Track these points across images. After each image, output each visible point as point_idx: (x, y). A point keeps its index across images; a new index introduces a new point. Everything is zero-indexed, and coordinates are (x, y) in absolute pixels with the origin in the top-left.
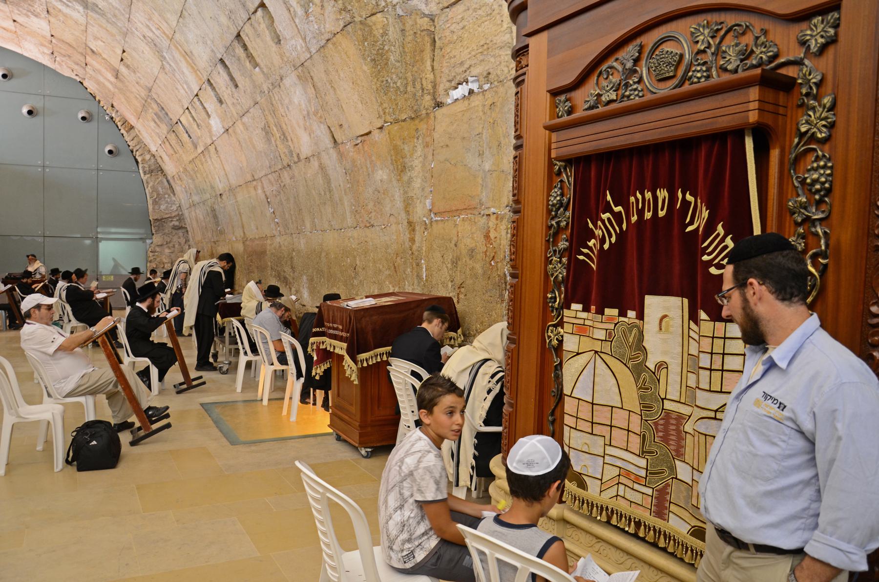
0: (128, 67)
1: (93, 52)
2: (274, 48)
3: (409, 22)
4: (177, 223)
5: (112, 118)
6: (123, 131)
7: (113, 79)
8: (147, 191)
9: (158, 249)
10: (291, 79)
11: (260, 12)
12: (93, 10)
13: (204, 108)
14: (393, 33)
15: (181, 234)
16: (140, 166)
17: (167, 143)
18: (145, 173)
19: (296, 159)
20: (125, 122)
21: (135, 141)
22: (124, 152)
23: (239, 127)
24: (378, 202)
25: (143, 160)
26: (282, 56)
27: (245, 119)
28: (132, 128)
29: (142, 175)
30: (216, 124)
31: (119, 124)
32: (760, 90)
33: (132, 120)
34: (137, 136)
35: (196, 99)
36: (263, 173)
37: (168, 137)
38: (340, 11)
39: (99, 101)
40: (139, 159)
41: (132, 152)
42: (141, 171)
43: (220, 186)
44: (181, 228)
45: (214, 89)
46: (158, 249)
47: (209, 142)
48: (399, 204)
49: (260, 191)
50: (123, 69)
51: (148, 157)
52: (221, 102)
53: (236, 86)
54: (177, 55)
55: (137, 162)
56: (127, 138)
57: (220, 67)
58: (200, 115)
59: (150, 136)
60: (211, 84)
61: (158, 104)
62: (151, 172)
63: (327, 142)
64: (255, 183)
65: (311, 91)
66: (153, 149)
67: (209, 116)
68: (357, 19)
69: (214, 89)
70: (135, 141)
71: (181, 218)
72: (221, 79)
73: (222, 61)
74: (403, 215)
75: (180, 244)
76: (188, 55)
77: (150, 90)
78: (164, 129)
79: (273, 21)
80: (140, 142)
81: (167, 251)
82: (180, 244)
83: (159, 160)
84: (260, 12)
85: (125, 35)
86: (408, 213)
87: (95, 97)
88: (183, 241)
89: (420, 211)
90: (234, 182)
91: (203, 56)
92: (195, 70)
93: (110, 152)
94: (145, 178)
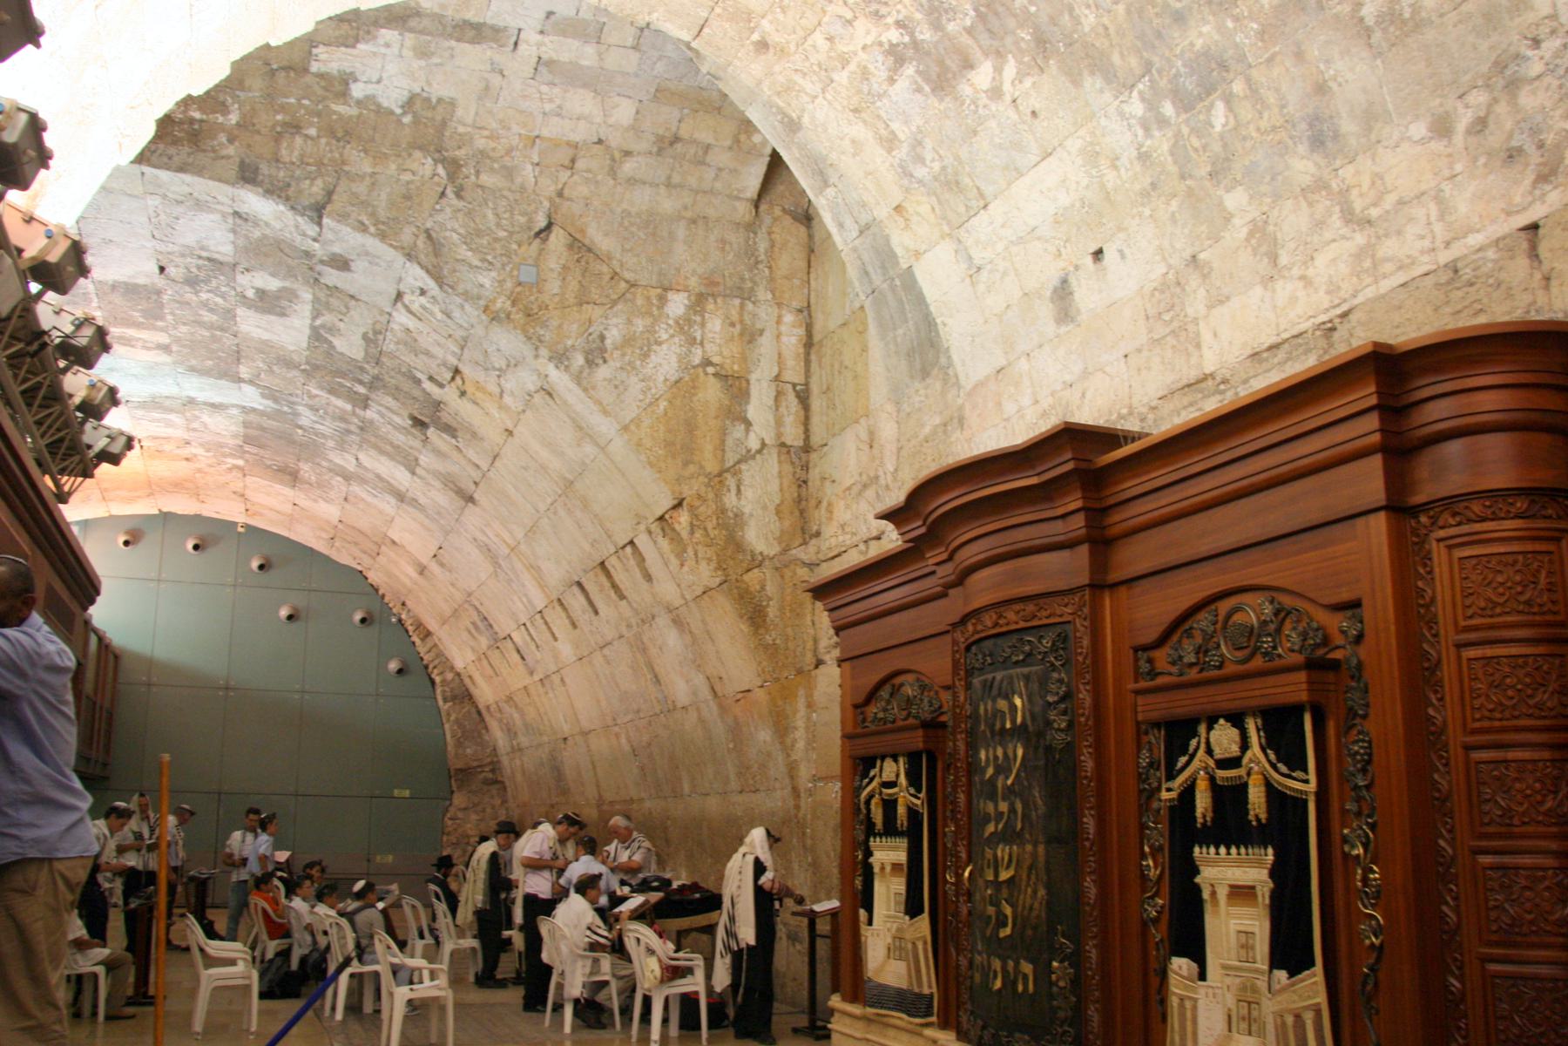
0: (442, 565)
1: (394, 542)
2: (645, 585)
3: (788, 573)
4: (490, 776)
5: (400, 620)
6: (415, 638)
7: (414, 575)
8: (447, 726)
9: (460, 815)
10: (663, 621)
11: (629, 549)
12: (409, 504)
13: (546, 623)
14: (770, 589)
15: (494, 792)
16: (439, 690)
17: (485, 662)
18: (445, 700)
19: (671, 708)
20: (419, 625)
21: (432, 654)
22: (417, 671)
23: (598, 659)
24: (763, 766)
25: (444, 681)
26: (654, 595)
27: (606, 651)
28: (428, 634)
29: (441, 703)
30: (566, 650)
31: (410, 628)
32: (1388, 519)
33: (432, 625)
34: (435, 645)
35: (538, 617)
36: (629, 717)
37: (489, 653)
38: (717, 569)
39: (383, 596)
40: (438, 679)
41: (426, 667)
42: (439, 698)
43: (566, 729)
44: (496, 782)
45: (565, 609)
46: (460, 815)
47: (553, 668)
48: (783, 769)
49: (623, 741)
50: (434, 567)
51: (450, 676)
52: (574, 626)
53: (596, 613)
54: (518, 566)
55: (433, 682)
56: (422, 649)
57: (576, 589)
58: (542, 635)
59: (460, 652)
60: (561, 604)
61: (479, 612)
62: (454, 698)
63: (705, 692)
64: (616, 729)
65: (688, 638)
66: (459, 664)
67: (556, 639)
68: (733, 577)
69: (565, 609)
70: (432, 654)
71: (495, 767)
72: (576, 602)
73: (579, 584)
74: (787, 781)
75: (493, 807)
76: (535, 569)
77: (470, 595)
78: (484, 642)
79: (644, 560)
80: (440, 654)
81: (474, 817)
82: (493, 807)
83: (467, 681)
84: (629, 549)
85: (447, 533)
86: (792, 778)
87: (377, 590)
88: (498, 802)
89: (804, 772)
90: (586, 725)
91: (555, 574)
92: (542, 586)
93: (196, 547)
94: (444, 707)
